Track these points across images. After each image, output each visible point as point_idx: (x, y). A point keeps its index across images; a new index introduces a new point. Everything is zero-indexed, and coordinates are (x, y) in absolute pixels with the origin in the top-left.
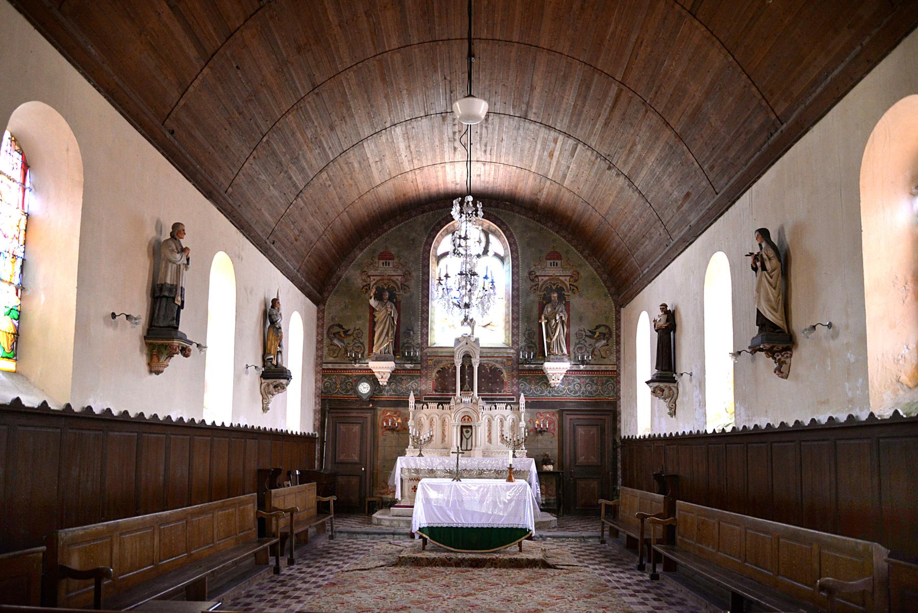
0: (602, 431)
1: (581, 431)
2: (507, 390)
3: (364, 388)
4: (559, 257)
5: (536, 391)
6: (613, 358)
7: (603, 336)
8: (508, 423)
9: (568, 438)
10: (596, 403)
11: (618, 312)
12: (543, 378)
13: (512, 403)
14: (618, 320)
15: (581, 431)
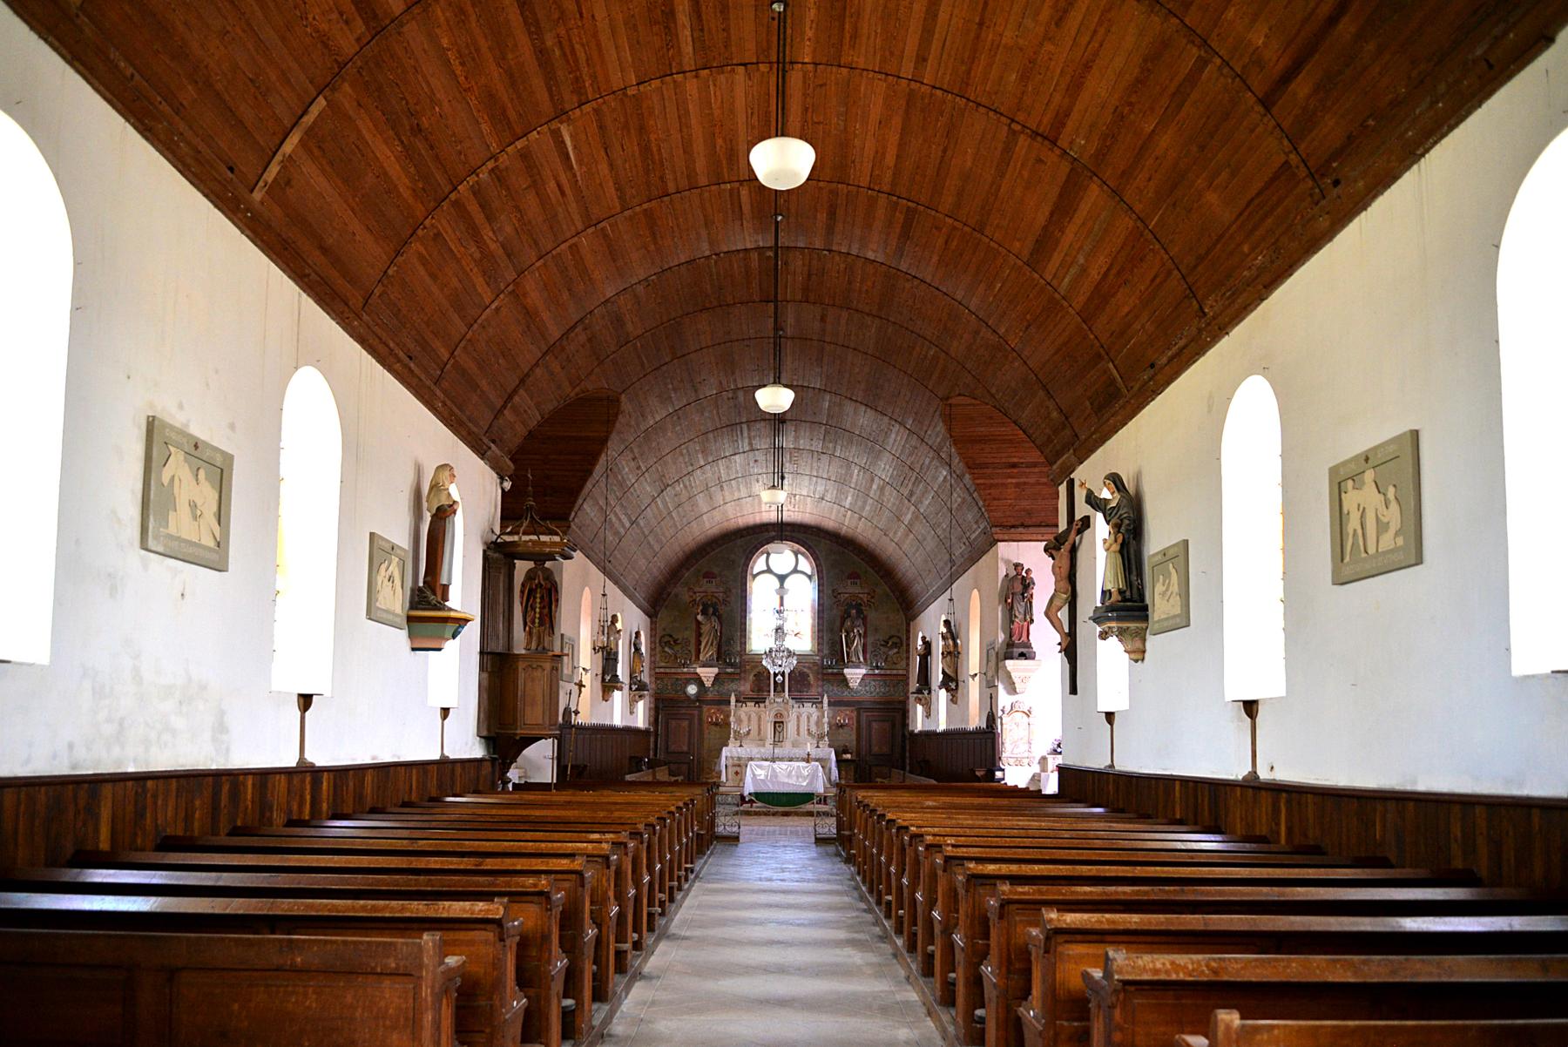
0: (893, 725)
1: (875, 725)
2: (814, 691)
3: (692, 690)
4: (858, 577)
5: (836, 690)
6: (904, 663)
7: (895, 645)
8: (814, 718)
9: (864, 733)
10: (889, 703)
11: (908, 625)
12: (844, 681)
13: (817, 702)
14: (908, 631)
15: (875, 725)
